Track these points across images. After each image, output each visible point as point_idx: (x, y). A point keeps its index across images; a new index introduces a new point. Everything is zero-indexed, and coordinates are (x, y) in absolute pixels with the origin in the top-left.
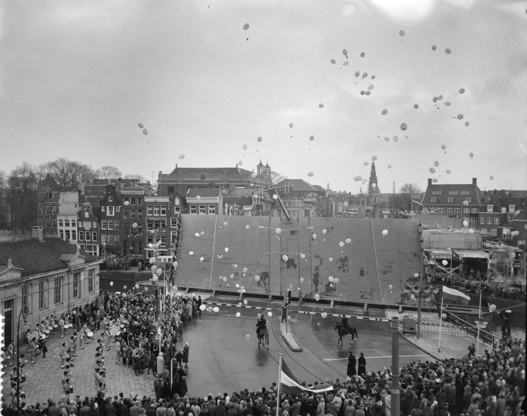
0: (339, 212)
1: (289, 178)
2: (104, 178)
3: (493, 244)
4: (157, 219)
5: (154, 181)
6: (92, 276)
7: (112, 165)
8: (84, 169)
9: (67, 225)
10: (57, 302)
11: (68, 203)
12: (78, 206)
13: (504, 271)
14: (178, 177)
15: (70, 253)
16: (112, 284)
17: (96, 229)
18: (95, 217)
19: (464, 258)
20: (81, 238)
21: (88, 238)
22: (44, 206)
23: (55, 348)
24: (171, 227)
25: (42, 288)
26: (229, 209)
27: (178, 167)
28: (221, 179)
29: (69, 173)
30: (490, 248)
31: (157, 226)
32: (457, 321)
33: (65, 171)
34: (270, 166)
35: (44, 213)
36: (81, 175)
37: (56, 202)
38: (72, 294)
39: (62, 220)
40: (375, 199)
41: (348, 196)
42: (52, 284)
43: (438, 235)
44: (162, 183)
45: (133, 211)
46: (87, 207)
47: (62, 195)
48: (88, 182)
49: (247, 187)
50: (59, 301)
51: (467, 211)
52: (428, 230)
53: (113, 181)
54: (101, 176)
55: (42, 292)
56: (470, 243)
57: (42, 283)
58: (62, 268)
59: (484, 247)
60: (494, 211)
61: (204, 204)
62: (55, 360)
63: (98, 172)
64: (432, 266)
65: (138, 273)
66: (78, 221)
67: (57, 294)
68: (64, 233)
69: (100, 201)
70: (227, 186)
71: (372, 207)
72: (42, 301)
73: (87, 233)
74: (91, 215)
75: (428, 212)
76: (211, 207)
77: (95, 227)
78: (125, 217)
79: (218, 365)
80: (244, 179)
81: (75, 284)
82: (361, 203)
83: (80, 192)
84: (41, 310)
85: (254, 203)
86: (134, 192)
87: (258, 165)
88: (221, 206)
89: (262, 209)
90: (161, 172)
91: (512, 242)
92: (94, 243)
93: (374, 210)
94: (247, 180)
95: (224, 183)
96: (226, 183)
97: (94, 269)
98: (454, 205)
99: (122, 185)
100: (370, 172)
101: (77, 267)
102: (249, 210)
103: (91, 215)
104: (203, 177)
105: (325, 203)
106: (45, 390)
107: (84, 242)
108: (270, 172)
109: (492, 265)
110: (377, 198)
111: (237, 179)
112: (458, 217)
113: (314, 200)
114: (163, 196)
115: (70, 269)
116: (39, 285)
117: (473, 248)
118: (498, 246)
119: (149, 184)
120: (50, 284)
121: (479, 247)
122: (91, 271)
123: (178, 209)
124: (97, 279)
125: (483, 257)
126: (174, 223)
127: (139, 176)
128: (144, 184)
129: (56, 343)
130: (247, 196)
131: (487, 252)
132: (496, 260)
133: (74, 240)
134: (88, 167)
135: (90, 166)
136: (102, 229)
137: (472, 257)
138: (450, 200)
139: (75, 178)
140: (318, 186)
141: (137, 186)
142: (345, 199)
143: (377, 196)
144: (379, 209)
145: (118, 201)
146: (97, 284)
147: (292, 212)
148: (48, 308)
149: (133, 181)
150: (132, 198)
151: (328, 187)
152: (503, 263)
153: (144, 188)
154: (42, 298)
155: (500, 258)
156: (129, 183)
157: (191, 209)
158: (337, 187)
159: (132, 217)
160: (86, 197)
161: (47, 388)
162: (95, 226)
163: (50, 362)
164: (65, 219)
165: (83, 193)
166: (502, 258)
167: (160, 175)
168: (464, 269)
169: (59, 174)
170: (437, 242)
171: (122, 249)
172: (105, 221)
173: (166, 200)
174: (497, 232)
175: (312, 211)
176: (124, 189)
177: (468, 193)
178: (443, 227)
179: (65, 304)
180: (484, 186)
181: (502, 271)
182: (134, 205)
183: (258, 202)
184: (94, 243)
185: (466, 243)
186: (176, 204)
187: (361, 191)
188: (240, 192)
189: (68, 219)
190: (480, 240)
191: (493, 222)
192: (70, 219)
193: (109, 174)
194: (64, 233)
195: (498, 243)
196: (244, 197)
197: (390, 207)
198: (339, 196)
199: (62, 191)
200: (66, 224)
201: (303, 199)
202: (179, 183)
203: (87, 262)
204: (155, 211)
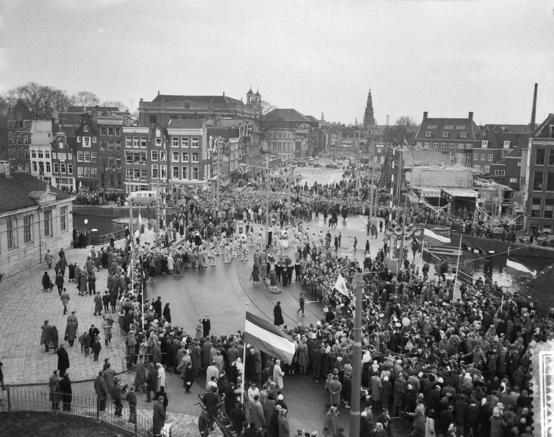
0: (332, 144)
1: (280, 107)
2: (80, 105)
3: (484, 182)
4: (137, 152)
5: (134, 109)
7: (90, 90)
8: (58, 95)
9: (41, 156)
10: (27, 241)
11: (40, 132)
12: (51, 136)
13: (493, 209)
14: (160, 105)
15: (40, 190)
16: (86, 221)
17: (72, 161)
18: (70, 148)
20: (56, 171)
21: (63, 170)
22: (15, 135)
23: (25, 289)
24: (152, 160)
25: (11, 227)
26: (213, 141)
27: (161, 94)
28: (206, 109)
30: (481, 186)
31: (137, 159)
33: (38, 97)
34: (261, 94)
35: (15, 143)
36: (55, 101)
38: (43, 233)
39: (35, 151)
40: (370, 131)
42: (21, 223)
43: (429, 172)
44: (143, 112)
45: (111, 142)
46: (62, 137)
47: (34, 124)
48: (63, 110)
49: (234, 117)
50: (30, 240)
51: (461, 146)
52: (419, 167)
53: (88, 108)
55: (10, 231)
56: (460, 181)
57: (11, 222)
58: (31, 206)
59: (474, 185)
60: (488, 148)
63: (74, 97)
64: (420, 205)
65: (117, 209)
66: (52, 152)
67: (27, 233)
68: (38, 164)
70: (213, 116)
71: (366, 140)
73: (62, 165)
74: (66, 145)
75: (422, 147)
76: (194, 139)
77: (70, 158)
78: (102, 149)
79: (195, 308)
80: (232, 109)
81: (47, 223)
82: (355, 136)
83: (53, 120)
84: (10, 250)
85: (242, 135)
86: (111, 121)
87: (247, 92)
88: (204, 138)
89: (250, 141)
90: (142, 99)
91: (503, 179)
92: (70, 176)
94: (234, 109)
95: (210, 113)
96: (212, 113)
97: (67, 206)
99: (100, 113)
100: (366, 102)
102: (236, 143)
103: (66, 145)
104: (187, 106)
106: (14, 333)
107: (59, 175)
108: (260, 101)
109: (480, 204)
110: (371, 130)
111: (224, 109)
112: (451, 153)
113: (306, 131)
114: (145, 126)
115: (40, 206)
116: (6, 224)
117: (463, 186)
118: (488, 184)
119: (127, 113)
120: (19, 223)
121: (470, 186)
122: (64, 209)
123: (159, 141)
124: (71, 217)
125: (472, 195)
126: (155, 156)
127: (119, 103)
128: (122, 113)
130: (233, 128)
131: (476, 190)
132: (485, 199)
134: (63, 92)
136: (78, 161)
137: (461, 195)
138: (445, 134)
139: (50, 104)
140: (310, 117)
141: (114, 115)
142: (338, 131)
143: (372, 128)
144: (373, 142)
145: (95, 130)
146: (70, 222)
148: (18, 248)
149: (110, 109)
151: (323, 117)
152: (492, 202)
153: (122, 117)
154: (11, 237)
155: (489, 196)
156: (106, 111)
157: (173, 141)
158: (331, 118)
160: (60, 126)
162: (70, 158)
163: (20, 304)
164: (38, 149)
165: (57, 122)
167: (141, 102)
169: (31, 100)
170: (428, 180)
171: (100, 183)
172: (81, 152)
173: (146, 131)
174: (490, 168)
175: (304, 143)
176: (101, 119)
177: (463, 127)
178: (435, 164)
179: (36, 243)
180: (479, 120)
181: (490, 210)
182: (112, 136)
184: (70, 176)
186: (157, 136)
187: (356, 122)
188: (227, 123)
189: (41, 150)
190: (471, 178)
191: (487, 159)
192: (43, 149)
194: (38, 164)
195: (488, 181)
196: (230, 128)
198: (333, 127)
199: (34, 119)
200: (39, 155)
201: (294, 130)
202: (162, 112)
203: (58, 199)
204: (135, 142)
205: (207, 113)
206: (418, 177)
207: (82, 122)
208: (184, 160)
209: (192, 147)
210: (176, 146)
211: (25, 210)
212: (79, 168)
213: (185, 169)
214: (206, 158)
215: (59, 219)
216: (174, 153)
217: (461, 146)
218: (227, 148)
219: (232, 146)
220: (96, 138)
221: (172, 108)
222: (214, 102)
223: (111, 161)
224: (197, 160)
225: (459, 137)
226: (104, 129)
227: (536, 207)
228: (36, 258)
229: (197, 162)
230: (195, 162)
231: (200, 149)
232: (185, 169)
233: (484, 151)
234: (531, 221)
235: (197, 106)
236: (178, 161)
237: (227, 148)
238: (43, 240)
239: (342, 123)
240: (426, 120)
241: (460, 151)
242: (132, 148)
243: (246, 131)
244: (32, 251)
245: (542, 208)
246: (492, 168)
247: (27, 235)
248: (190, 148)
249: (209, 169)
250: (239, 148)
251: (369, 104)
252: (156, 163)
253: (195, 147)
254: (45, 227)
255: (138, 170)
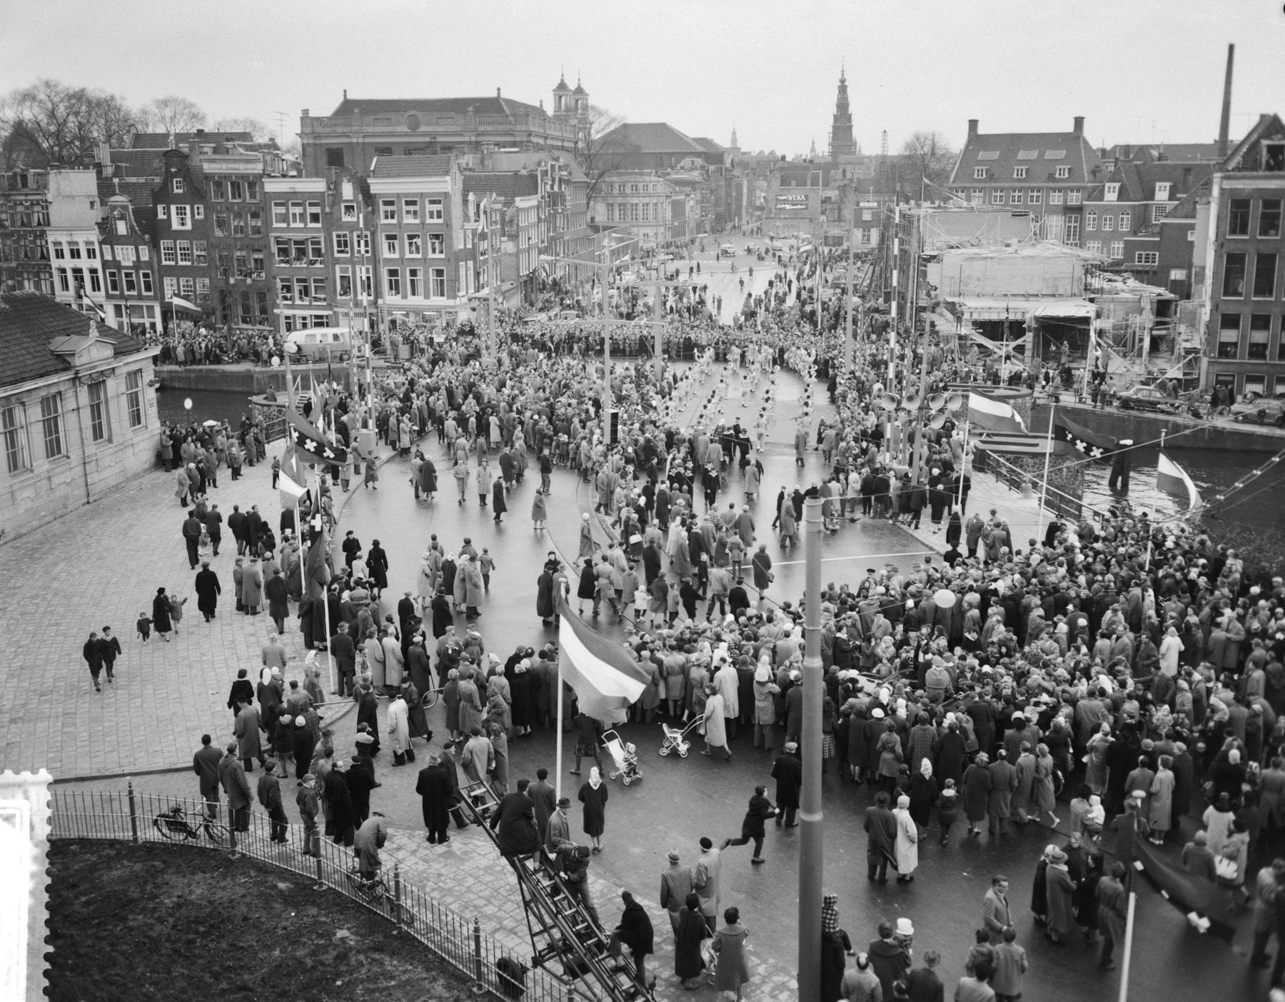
0: (758, 203)
1: (632, 120)
2: (161, 130)
4: (299, 236)
5: (289, 136)
6: (137, 386)
7: (180, 94)
8: (105, 107)
9: (75, 254)
10: (53, 455)
11: (71, 197)
12: (97, 205)
13: (1129, 344)
14: (350, 125)
17: (149, 264)
18: (144, 233)
19: (1037, 319)
21: (131, 285)
22: (11, 208)
23: (56, 564)
24: (337, 255)
25: (12, 423)
26: (478, 206)
27: (350, 97)
29: (71, 118)
30: (1101, 291)
32: (1004, 471)
35: (13, 225)
37: (39, 197)
38: (89, 433)
39: (60, 243)
40: (844, 171)
41: (778, 165)
42: (35, 413)
43: (981, 262)
44: (311, 141)
45: (238, 215)
46: (122, 207)
50: (59, 452)
51: (1056, 199)
52: (960, 251)
53: (180, 137)
54: (154, 125)
55: (11, 432)
57: (10, 411)
58: (56, 371)
59: (1087, 288)
61: (415, 195)
62: (56, 594)
66: (101, 243)
67: (50, 434)
68: (70, 275)
69: (153, 190)
71: (837, 192)
72: (14, 454)
73: (127, 275)
75: (965, 204)
76: (432, 202)
77: (145, 257)
80: (518, 128)
81: (96, 410)
82: (809, 182)
83: (99, 167)
85: (544, 188)
86: (236, 166)
87: (554, 87)
88: (457, 199)
89: (564, 201)
90: (306, 112)
91: (1155, 273)
92: (148, 298)
93: (841, 199)
94: (524, 128)
95: (467, 139)
96: (473, 139)
97: (140, 370)
98: (1027, 185)
99: (208, 148)
101: (95, 367)
102: (531, 208)
103: (132, 228)
104: (414, 125)
105: (723, 183)
108: (585, 107)
110: (848, 168)
111: (500, 128)
112: (1032, 216)
113: (696, 176)
115: (77, 373)
117: (1061, 291)
119: (273, 145)
122: (134, 376)
123: (349, 209)
125: (1081, 313)
126: (343, 244)
127: (252, 123)
128: (259, 145)
129: (57, 553)
130: (524, 172)
131: (1092, 300)
133: (97, 293)
135: (123, 98)
136: (164, 263)
138: (1018, 171)
141: (241, 150)
142: (771, 171)
144: (852, 197)
145: (198, 188)
146: (151, 405)
147: (640, 207)
148: (32, 471)
149: (230, 137)
150: (233, 184)
151: (734, 140)
153: (260, 156)
156: (221, 142)
157: (382, 208)
158: (754, 143)
159: (236, 232)
160: (116, 180)
161: (38, 663)
163: (45, 599)
165: (109, 171)
166: (1127, 314)
167: (305, 118)
168: (1036, 345)
170: (979, 279)
171: (218, 313)
173: (318, 185)
175: (692, 203)
177: (1061, 154)
178: (996, 243)
179: (73, 457)
180: (1099, 137)
181: (1125, 346)
183: (552, 187)
184: (148, 298)
185: (1044, 280)
187: (813, 150)
188: (510, 161)
190: (1079, 272)
192: (81, 239)
193: (173, 119)
194: (70, 275)
196: (516, 173)
197: (878, 192)
198: (759, 163)
199: (53, 167)
200: (72, 251)
201: (668, 174)
202: (354, 140)
203: (119, 353)
204: (294, 215)
205: (460, 139)
206: (957, 275)
207: (168, 171)
208: (411, 252)
209: (429, 221)
210: (390, 221)
211: (41, 383)
212: (167, 281)
213: (413, 273)
214: (462, 247)
215: (124, 401)
216: (389, 237)
217: (1056, 199)
218: (511, 221)
219: (522, 217)
220: (201, 206)
221: (378, 129)
222: (477, 111)
223: (242, 261)
224: (441, 252)
225: (1051, 178)
226: (219, 184)
227: (1229, 336)
228: (76, 492)
229: (442, 256)
230: (438, 255)
231: (448, 225)
232: (413, 273)
233: (1109, 209)
234: (1217, 369)
235: (437, 124)
236: (396, 256)
237: (511, 221)
238: (91, 448)
239: (779, 154)
240: (976, 140)
241: (1052, 210)
242: (288, 229)
243: (553, 180)
244: (67, 477)
245: (1244, 337)
246: (1130, 248)
247: (51, 441)
248: (423, 223)
249: (471, 272)
250: (539, 220)
251: (843, 105)
252: (346, 261)
253: (436, 221)
254: (93, 419)
255: (304, 281)
